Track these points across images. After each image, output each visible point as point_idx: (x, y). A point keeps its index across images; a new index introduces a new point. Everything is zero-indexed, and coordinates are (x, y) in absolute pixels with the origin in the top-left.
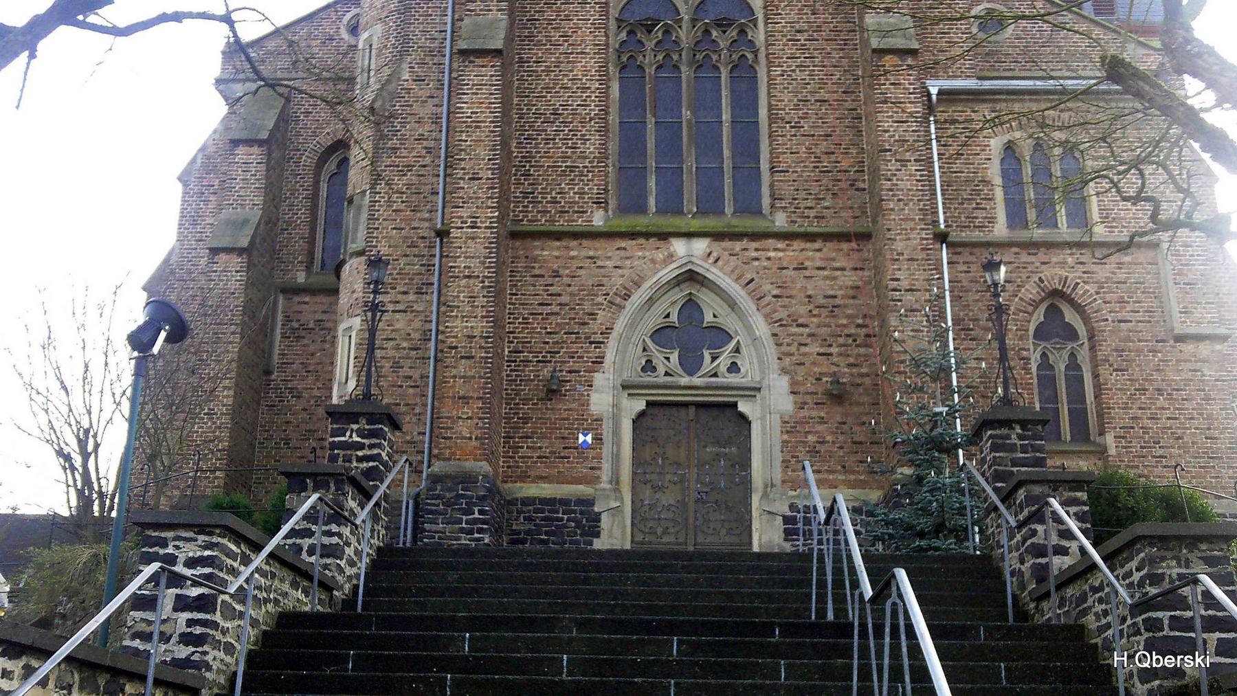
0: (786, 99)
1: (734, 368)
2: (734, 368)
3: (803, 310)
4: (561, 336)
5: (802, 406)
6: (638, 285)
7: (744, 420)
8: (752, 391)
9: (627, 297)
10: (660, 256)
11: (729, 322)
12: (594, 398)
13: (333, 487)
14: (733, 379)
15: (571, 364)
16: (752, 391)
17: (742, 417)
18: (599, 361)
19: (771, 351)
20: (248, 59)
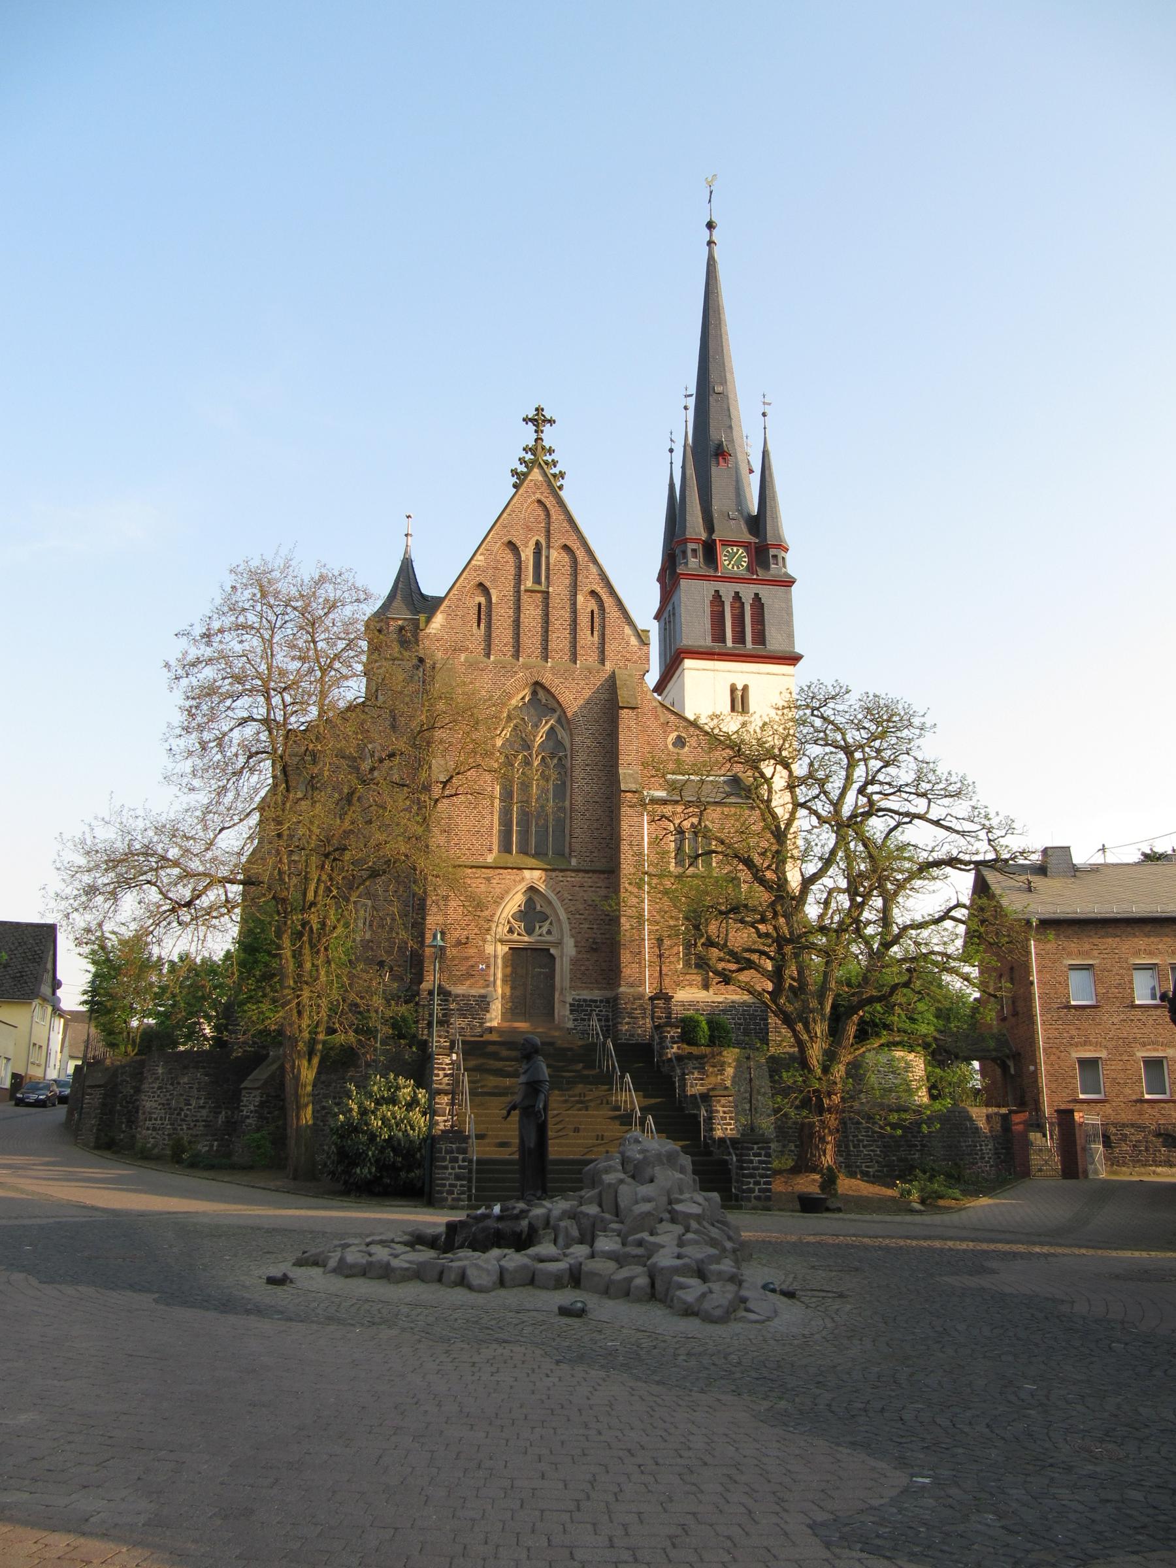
5: (579, 952)
6: (507, 892)
10: (518, 879)
11: (548, 911)
14: (548, 938)
20: (545, 474)
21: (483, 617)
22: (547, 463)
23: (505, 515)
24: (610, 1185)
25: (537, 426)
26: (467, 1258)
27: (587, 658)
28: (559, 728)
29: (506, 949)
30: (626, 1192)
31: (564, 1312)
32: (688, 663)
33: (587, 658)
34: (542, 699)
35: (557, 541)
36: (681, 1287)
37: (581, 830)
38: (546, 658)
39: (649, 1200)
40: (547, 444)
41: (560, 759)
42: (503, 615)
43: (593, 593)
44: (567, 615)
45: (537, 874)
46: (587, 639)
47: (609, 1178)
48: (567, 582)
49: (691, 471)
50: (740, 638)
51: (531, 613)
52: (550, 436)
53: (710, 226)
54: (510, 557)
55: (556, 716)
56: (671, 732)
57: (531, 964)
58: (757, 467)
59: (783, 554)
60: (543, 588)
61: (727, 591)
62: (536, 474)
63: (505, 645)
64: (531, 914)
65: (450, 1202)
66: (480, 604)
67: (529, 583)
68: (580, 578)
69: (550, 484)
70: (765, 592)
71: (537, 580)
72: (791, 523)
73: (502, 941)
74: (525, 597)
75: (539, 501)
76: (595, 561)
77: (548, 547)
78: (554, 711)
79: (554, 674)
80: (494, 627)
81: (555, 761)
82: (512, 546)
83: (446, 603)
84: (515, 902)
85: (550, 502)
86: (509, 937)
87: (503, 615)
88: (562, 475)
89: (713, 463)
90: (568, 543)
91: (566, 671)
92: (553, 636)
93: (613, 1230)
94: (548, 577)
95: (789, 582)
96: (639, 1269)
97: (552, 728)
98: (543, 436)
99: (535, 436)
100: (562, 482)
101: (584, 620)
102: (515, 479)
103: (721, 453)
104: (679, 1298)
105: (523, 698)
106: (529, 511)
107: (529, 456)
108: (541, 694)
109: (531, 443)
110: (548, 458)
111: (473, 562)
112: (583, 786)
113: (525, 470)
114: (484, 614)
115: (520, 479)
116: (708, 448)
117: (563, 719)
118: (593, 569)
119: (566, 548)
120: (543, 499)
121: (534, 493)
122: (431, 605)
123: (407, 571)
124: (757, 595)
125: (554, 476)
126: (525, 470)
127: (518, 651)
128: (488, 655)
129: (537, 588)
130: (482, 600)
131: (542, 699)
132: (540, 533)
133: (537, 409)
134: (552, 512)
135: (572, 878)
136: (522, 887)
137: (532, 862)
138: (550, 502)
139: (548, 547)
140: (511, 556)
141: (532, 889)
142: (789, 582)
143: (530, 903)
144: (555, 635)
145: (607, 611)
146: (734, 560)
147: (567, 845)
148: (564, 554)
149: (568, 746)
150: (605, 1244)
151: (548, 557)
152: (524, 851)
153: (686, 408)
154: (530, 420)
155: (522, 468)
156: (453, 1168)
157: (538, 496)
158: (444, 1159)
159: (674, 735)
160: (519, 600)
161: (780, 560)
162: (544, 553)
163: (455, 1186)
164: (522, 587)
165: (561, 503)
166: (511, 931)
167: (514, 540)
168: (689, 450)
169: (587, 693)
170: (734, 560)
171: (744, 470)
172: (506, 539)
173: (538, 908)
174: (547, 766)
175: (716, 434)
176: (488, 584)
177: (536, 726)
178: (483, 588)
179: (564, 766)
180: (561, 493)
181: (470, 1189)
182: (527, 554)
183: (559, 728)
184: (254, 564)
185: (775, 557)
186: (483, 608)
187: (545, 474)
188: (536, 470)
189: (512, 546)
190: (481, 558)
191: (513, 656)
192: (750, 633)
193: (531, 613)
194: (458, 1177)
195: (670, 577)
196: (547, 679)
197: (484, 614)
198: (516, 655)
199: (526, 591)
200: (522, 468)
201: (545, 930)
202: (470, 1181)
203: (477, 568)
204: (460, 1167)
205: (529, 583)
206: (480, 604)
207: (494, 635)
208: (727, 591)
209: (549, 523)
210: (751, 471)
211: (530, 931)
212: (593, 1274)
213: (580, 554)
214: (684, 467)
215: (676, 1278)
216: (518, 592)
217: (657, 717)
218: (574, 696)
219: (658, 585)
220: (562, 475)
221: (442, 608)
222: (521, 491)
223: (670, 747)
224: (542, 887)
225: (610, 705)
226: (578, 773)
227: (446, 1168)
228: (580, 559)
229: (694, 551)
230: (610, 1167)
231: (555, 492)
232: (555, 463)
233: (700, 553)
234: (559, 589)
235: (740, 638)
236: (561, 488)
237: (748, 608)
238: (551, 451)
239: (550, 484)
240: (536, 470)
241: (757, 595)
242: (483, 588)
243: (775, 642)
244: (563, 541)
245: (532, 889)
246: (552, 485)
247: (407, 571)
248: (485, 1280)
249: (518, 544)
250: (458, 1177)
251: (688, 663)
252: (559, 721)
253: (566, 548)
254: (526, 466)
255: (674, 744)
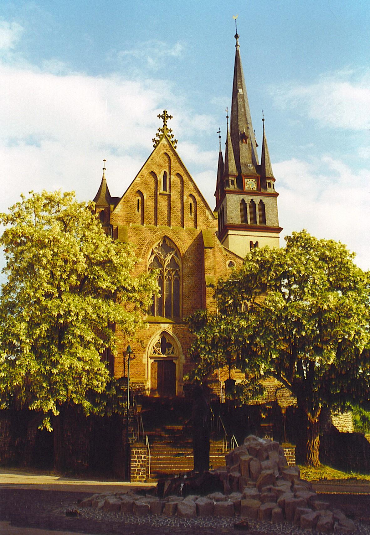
0: (186, 290)
1: (173, 353)
2: (173, 353)
3: (188, 340)
4: (136, 346)
5: (187, 362)
6: (153, 334)
7: (175, 364)
8: (177, 358)
9: (150, 337)
10: (158, 328)
11: (172, 343)
12: (143, 360)
13: (87, 326)
14: (172, 355)
15: (138, 352)
16: (177, 358)
17: (174, 363)
18: (144, 352)
19: (181, 350)
20: (168, 141)
21: (140, 206)
22: (169, 136)
23: (150, 159)
24: (245, 461)
25: (164, 119)
26: (176, 500)
27: (189, 224)
28: (176, 257)
29: (153, 361)
30: (254, 464)
31: (236, 526)
32: (230, 232)
33: (189, 224)
34: (168, 244)
35: (174, 172)
36: (303, 512)
37: (186, 303)
38: (169, 225)
39: (269, 469)
40: (169, 127)
41: (177, 272)
42: (149, 204)
43: (191, 195)
44: (179, 205)
45: (167, 325)
46: (189, 217)
47: (243, 458)
48: (179, 190)
49: (230, 146)
50: (254, 220)
51: (162, 204)
52: (170, 124)
53: (236, 36)
54: (152, 179)
55: (174, 252)
56: (228, 260)
57: (164, 367)
58: (260, 144)
59: (272, 182)
60: (168, 193)
61: (248, 199)
62: (164, 141)
63: (150, 219)
64: (165, 343)
65: (138, 478)
66: (138, 200)
67: (161, 190)
68: (185, 188)
69: (170, 145)
70: (266, 200)
71: (165, 189)
72: (276, 169)
73: (151, 358)
74: (159, 197)
75: (165, 153)
76: (191, 180)
77: (170, 174)
78: (173, 249)
79: (173, 233)
80: (145, 211)
81: (174, 272)
82: (153, 174)
83: (122, 201)
84: (156, 339)
85: (170, 154)
86: (155, 355)
87: (149, 204)
88: (176, 141)
89: (240, 142)
90: (179, 172)
91: (179, 231)
92: (172, 215)
93: (250, 484)
94: (170, 188)
95: (276, 195)
96: (273, 504)
97: (173, 257)
98: (166, 123)
99: (163, 124)
100: (176, 145)
101: (187, 207)
102: (154, 143)
103: (244, 137)
104: (304, 519)
105: (159, 244)
106: (159, 157)
107: (160, 133)
108: (167, 241)
109: (162, 127)
110: (170, 134)
111: (135, 181)
112: (187, 285)
113: (159, 139)
114: (141, 205)
115: (157, 143)
116: (238, 136)
117: (178, 253)
118: (191, 184)
119: (178, 175)
120: (167, 152)
121: (163, 150)
122: (116, 201)
123: (103, 185)
124: (261, 200)
125: (172, 142)
126: (159, 139)
127: (157, 222)
128: (143, 224)
129: (165, 192)
130: (140, 198)
131: (168, 244)
132: (165, 171)
133: (164, 112)
134: (172, 158)
135: (183, 327)
136: (160, 332)
137: (164, 319)
138: (170, 154)
139: (170, 174)
140: (153, 178)
141: (164, 333)
142: (276, 195)
143: (163, 339)
144: (174, 215)
145: (198, 203)
146: (250, 184)
147: (181, 312)
148: (177, 178)
149: (180, 266)
150: (251, 491)
151: (170, 179)
152: (160, 314)
153: (227, 117)
154: (162, 116)
155: (157, 138)
156: (139, 462)
157: (165, 151)
158: (135, 457)
159: (228, 262)
160: (157, 198)
161: (272, 186)
162: (168, 177)
163: (140, 470)
164: (158, 193)
165: (176, 154)
166: (155, 352)
167: (154, 171)
168: (229, 135)
169: (190, 242)
170: (250, 184)
171: (254, 145)
172: (150, 171)
173: (167, 341)
174: (171, 275)
175: (242, 129)
176: (142, 191)
177: (165, 257)
178: (140, 193)
179: (179, 275)
180: (176, 150)
181: (148, 472)
182: (160, 177)
183: (176, 257)
184: (29, 197)
185: (270, 184)
186: (140, 202)
187: (168, 141)
188: (164, 139)
189: (153, 174)
190: (139, 179)
191: (154, 224)
192: (257, 219)
193: (162, 204)
194: (142, 466)
195: (221, 193)
196: (170, 234)
197: (141, 205)
198: (156, 224)
199: (160, 194)
200: (157, 138)
201: (171, 351)
202: (148, 468)
203: (137, 184)
204: (142, 461)
205: (161, 190)
206: (138, 200)
207: (145, 214)
208: (248, 199)
209: (170, 163)
210: (257, 146)
211: (163, 352)
212: (246, 507)
213: (185, 178)
214: (227, 144)
215: (298, 508)
216: (157, 194)
217: (221, 252)
218: (184, 243)
219: (215, 197)
220: (176, 141)
221: (121, 202)
222: (157, 149)
223: (227, 266)
224: (171, 332)
225: (200, 246)
226: (186, 278)
227: (136, 461)
228: (185, 180)
229: (232, 181)
230: (242, 452)
231: (173, 149)
232: (172, 136)
233: (235, 182)
234: (175, 193)
235: (254, 220)
236: (175, 147)
237: (257, 206)
238: (171, 131)
239: (170, 145)
240: (164, 139)
241: (261, 200)
242: (140, 193)
243: (268, 224)
244: (176, 172)
245: (164, 333)
246: (172, 146)
247: (103, 185)
248: (190, 511)
249: (156, 173)
250: (142, 466)
251: (230, 232)
252: (176, 254)
253: (178, 175)
254: (160, 137)
255: (229, 266)
